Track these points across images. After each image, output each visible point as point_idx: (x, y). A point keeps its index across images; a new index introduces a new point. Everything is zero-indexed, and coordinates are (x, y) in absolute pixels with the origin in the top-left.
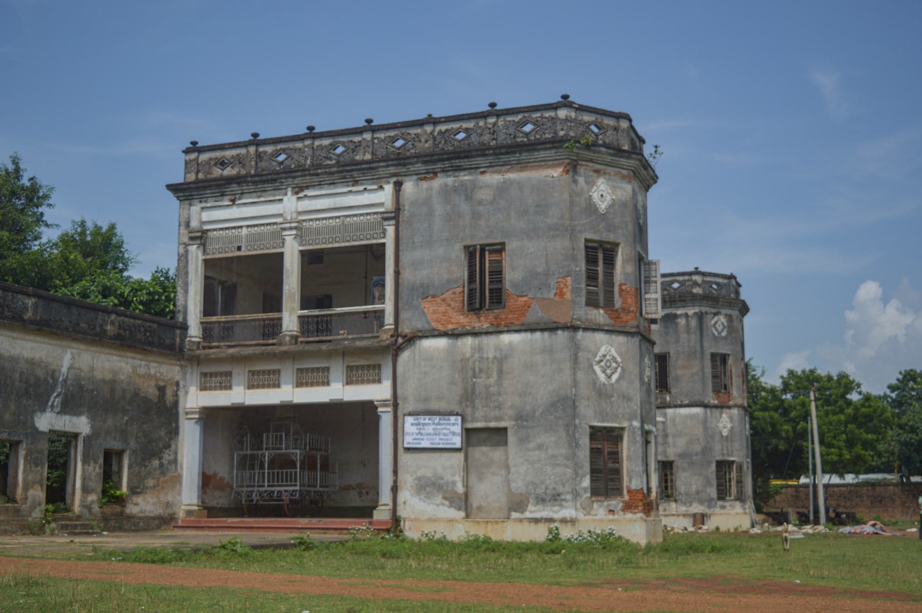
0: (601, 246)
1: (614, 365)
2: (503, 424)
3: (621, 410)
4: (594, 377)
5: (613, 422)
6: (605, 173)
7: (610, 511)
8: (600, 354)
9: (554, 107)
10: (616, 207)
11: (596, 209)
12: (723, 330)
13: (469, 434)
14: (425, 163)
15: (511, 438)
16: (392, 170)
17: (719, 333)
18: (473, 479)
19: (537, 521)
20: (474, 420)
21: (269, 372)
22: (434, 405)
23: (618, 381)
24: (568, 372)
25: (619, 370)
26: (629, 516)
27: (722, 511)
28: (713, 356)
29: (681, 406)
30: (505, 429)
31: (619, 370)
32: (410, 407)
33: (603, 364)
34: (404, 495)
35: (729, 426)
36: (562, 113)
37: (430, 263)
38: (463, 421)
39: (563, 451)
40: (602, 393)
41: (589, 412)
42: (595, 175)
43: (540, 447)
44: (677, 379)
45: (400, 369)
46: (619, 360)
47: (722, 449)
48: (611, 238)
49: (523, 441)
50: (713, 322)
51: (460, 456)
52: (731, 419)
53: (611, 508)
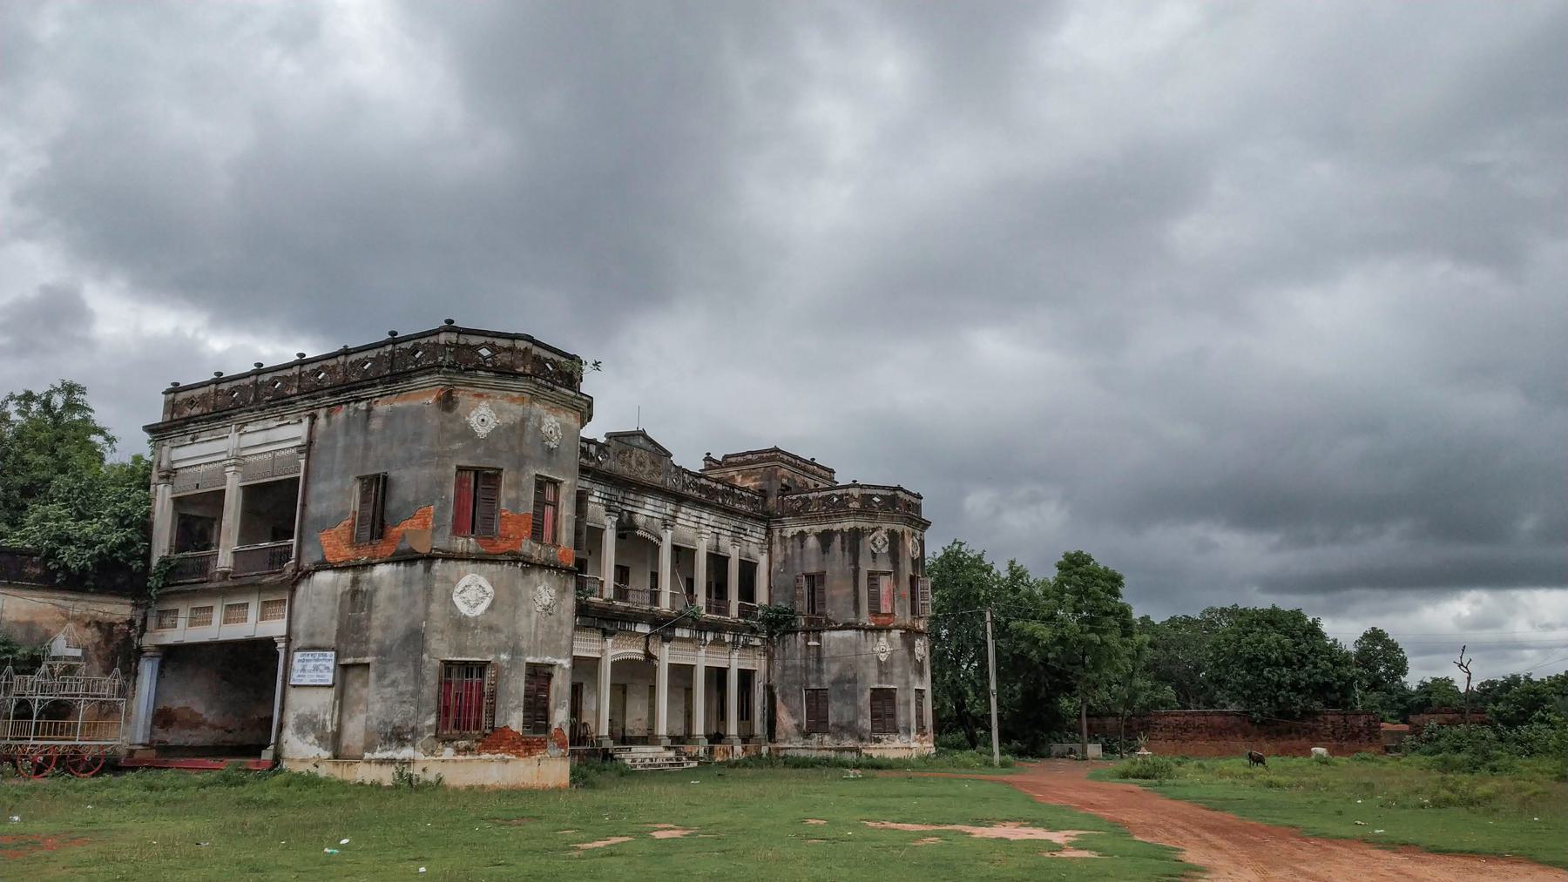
2: (367, 660)
9: (436, 332)
13: (343, 669)
14: (332, 395)
15: (372, 675)
16: (307, 403)
18: (346, 716)
19: (381, 762)
20: (346, 656)
21: (239, 605)
22: (319, 641)
24: (421, 604)
30: (368, 665)
32: (299, 643)
34: (288, 734)
36: (443, 338)
37: (333, 499)
38: (337, 658)
39: (411, 688)
40: (461, 624)
41: (443, 646)
43: (393, 683)
44: (833, 598)
45: (297, 604)
48: (492, 463)
49: (381, 676)
51: (332, 692)
52: (890, 642)
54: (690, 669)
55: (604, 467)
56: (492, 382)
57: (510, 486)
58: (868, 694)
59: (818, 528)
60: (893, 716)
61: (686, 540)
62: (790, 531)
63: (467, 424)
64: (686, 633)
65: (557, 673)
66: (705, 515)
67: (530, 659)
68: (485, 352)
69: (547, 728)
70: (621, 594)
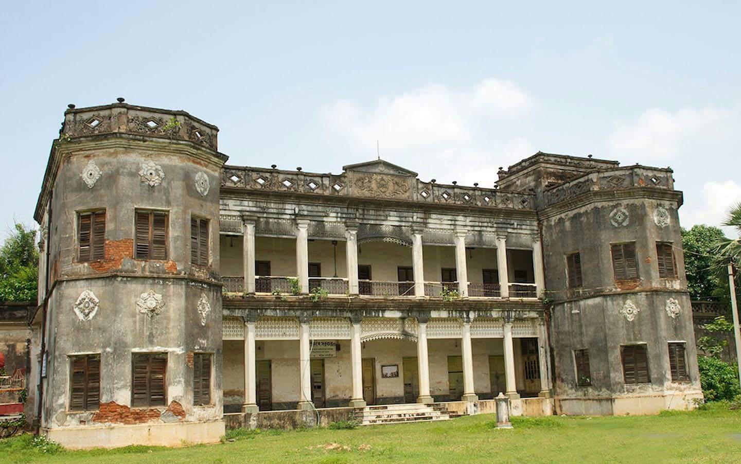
0: (93, 213)
1: (92, 305)
3: (96, 340)
4: (74, 317)
5: (89, 350)
6: (94, 156)
7: (81, 422)
8: (80, 299)
10: (103, 180)
11: (86, 185)
12: (624, 220)
17: (620, 224)
23: (94, 317)
25: (96, 308)
26: (98, 425)
27: (630, 395)
28: (615, 248)
29: (588, 298)
31: (96, 308)
33: (82, 306)
35: (635, 312)
42: (86, 160)
46: (97, 300)
47: (628, 334)
50: (611, 214)
52: (637, 304)
53: (82, 419)
54: (457, 343)
55: (341, 194)
56: (92, 144)
57: (188, 219)
58: (618, 352)
59: (571, 214)
60: (647, 368)
61: (442, 241)
62: (554, 220)
63: (81, 178)
64: (444, 314)
65: (171, 364)
66: (460, 218)
67: (136, 350)
68: (152, 124)
69: (163, 401)
70: (365, 288)
